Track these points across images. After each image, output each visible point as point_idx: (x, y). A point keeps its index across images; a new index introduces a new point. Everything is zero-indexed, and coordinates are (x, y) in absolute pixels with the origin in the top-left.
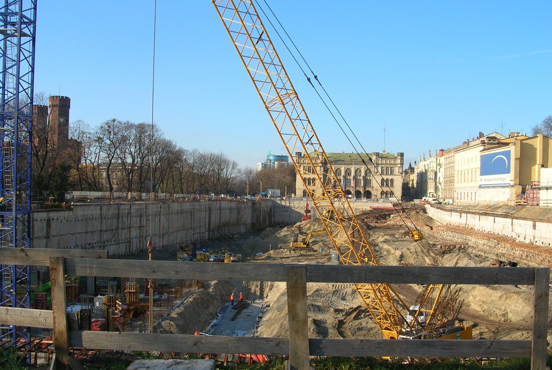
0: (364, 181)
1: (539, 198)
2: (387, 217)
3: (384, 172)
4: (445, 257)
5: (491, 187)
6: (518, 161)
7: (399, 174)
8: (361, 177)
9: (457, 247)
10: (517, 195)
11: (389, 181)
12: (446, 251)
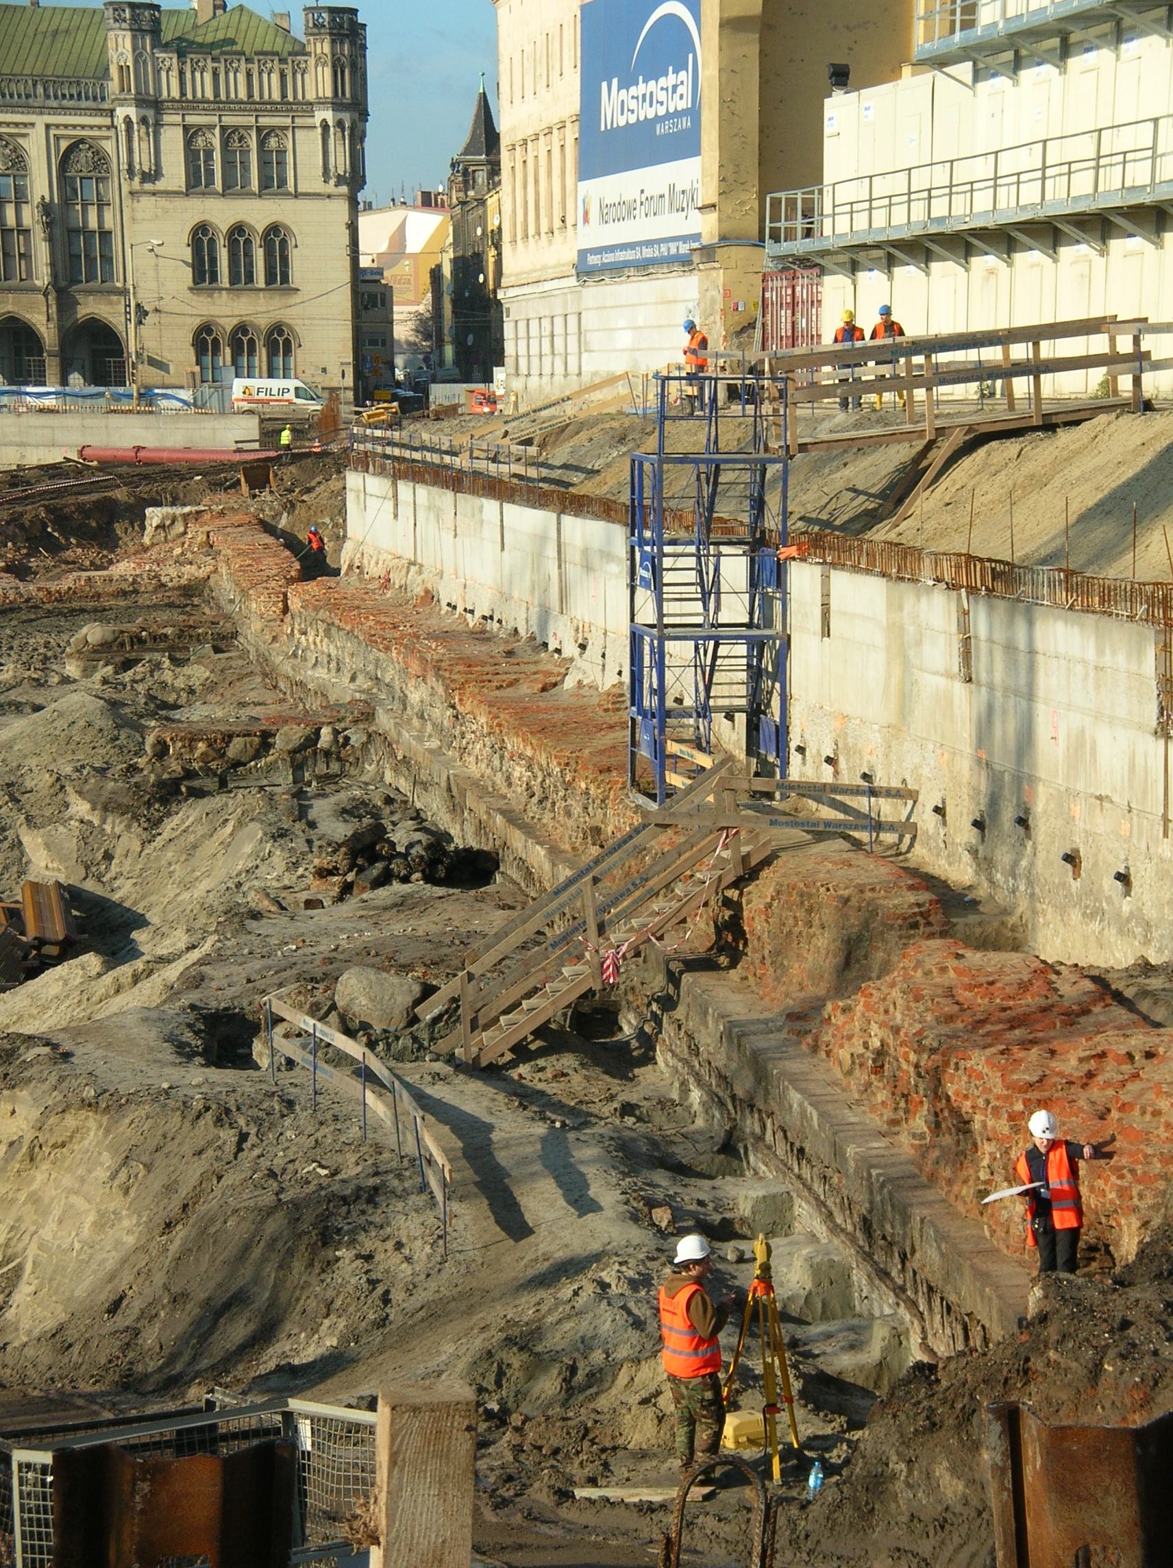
0: (50, 240)
1: (819, 336)
2: (118, 528)
3: (210, 173)
4: (169, 827)
5: (626, 265)
6: (751, 48)
7: (330, 188)
8: (26, 211)
9: (279, 741)
10: (739, 320)
11: (257, 241)
12: (189, 774)
